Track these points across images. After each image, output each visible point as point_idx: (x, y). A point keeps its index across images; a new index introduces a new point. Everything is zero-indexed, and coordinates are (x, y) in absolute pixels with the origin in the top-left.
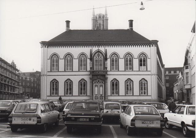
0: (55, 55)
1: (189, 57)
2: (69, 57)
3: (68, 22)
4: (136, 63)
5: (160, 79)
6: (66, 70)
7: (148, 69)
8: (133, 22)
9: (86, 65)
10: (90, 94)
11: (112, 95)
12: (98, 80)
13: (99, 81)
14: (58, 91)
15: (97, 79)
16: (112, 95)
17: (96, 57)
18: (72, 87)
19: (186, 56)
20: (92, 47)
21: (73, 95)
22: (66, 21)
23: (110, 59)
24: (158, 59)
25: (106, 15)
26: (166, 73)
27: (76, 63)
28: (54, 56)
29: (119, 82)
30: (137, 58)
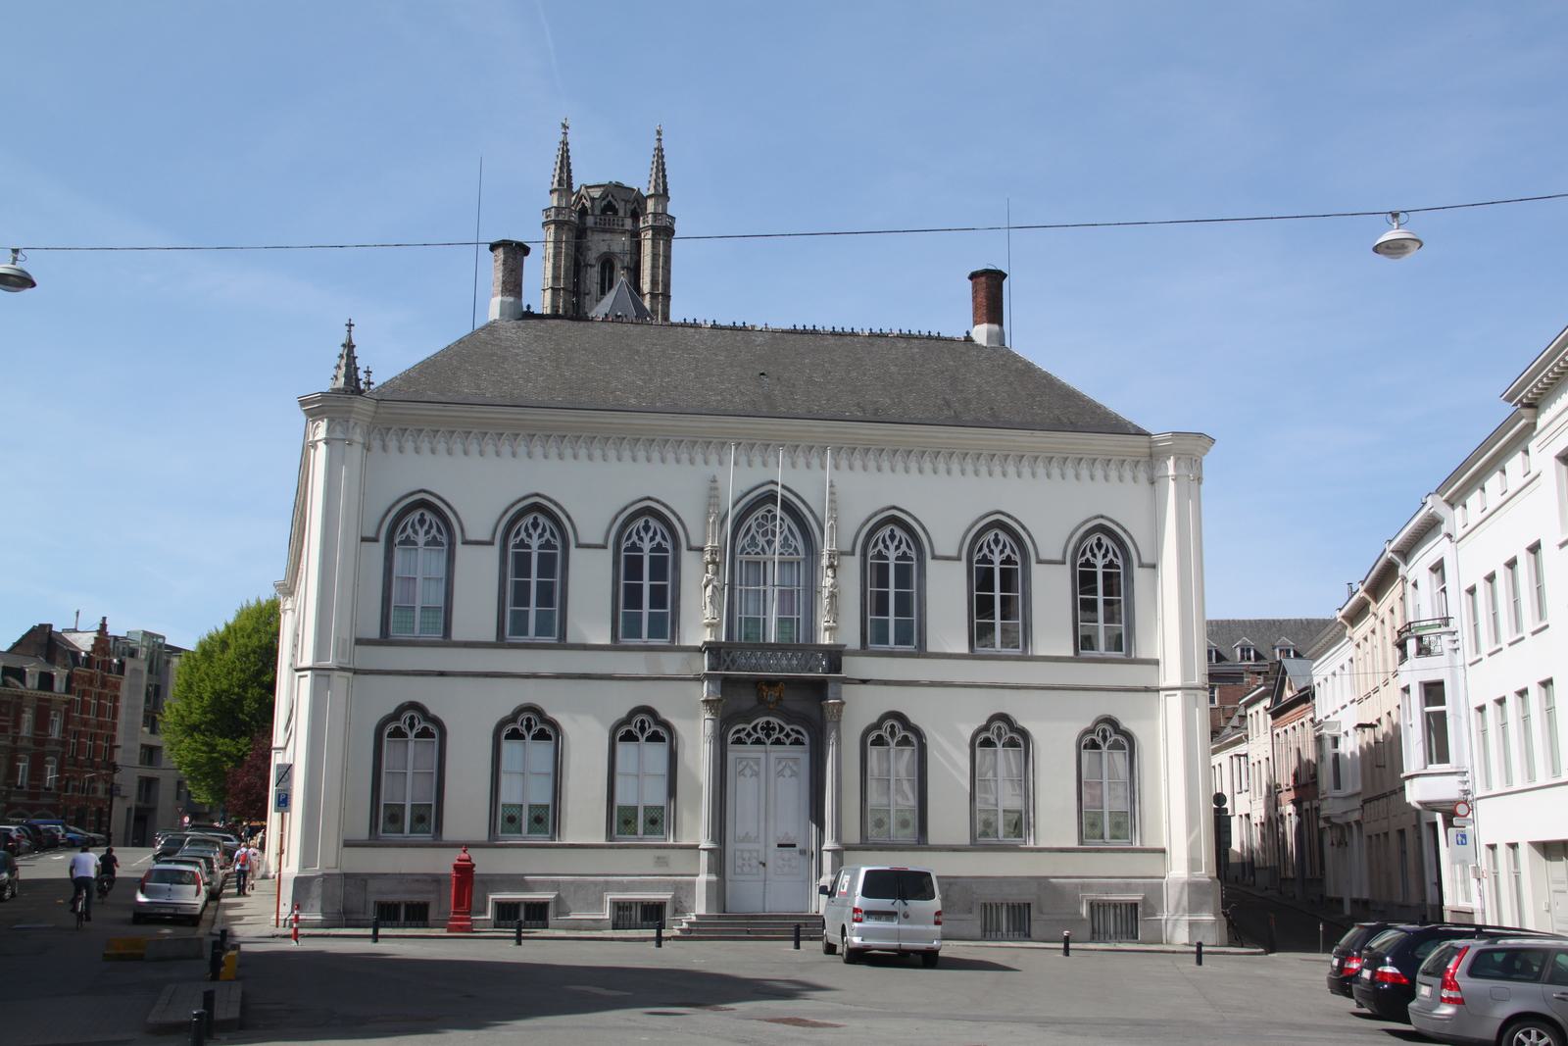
6: (510, 638)
12: (762, 720)
17: (753, 542)
23: (856, 560)
25: (662, 195)
28: (529, 519)
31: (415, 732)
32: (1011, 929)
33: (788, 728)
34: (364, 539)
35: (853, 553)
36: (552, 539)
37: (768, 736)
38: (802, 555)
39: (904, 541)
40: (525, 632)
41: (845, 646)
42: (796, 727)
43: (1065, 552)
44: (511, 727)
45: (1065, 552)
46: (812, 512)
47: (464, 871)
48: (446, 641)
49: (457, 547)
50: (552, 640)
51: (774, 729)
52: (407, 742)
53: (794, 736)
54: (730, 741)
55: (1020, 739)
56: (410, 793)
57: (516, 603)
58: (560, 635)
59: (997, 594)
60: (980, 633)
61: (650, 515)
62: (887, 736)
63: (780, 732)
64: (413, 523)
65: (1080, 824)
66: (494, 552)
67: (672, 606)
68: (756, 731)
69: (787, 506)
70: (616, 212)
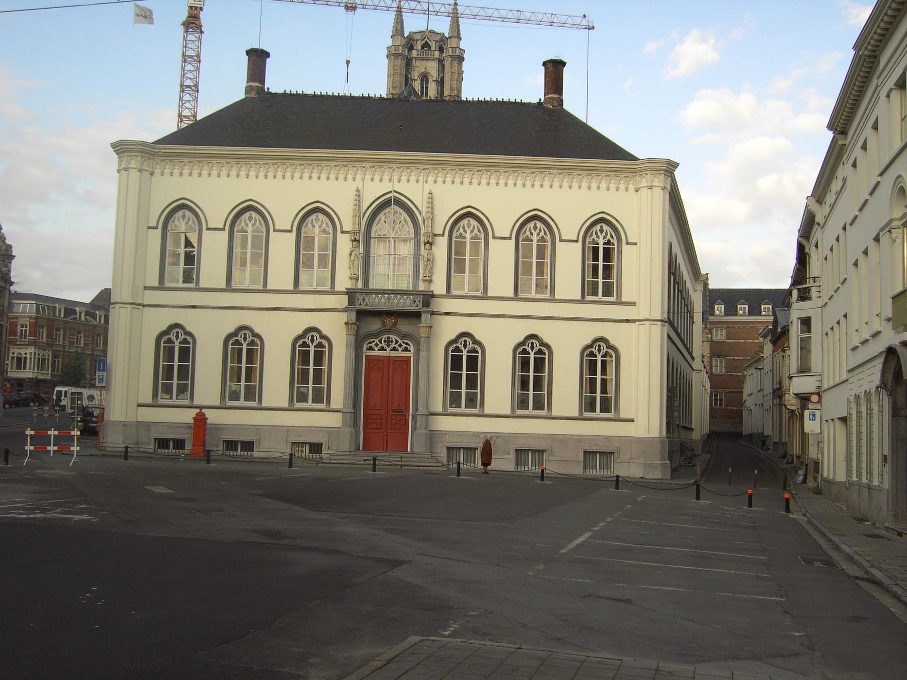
0: (248, 208)
1: (817, 246)
3: (258, 59)
5: (682, 341)
8: (567, 73)
10: (344, 404)
11: (451, 410)
13: (389, 342)
14: (581, 395)
16: (451, 410)
19: (803, 241)
20: (363, 179)
21: (487, 411)
22: (248, 53)
24: (677, 250)
26: (713, 314)
30: (510, 238)
33: (400, 341)
34: (149, 228)
35: (443, 235)
44: (167, 337)
46: (417, 209)
47: (200, 420)
48: (485, 297)
50: (192, 285)
51: (392, 341)
53: (404, 345)
70: (430, 47)
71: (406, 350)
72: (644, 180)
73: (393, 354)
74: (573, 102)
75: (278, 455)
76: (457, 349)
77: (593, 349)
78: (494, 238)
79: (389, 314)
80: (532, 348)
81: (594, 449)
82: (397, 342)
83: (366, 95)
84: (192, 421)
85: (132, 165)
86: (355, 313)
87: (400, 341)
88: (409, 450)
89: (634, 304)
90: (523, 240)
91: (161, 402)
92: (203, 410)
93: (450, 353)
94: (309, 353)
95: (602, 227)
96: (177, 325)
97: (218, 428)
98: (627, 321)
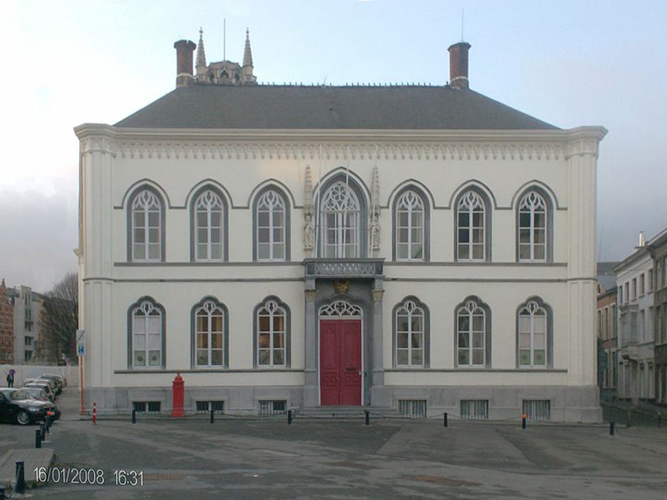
2: (210, 198)
4: (503, 228)
7: (449, 261)
9: (284, 236)
11: (399, 367)
15: (335, 299)
16: (399, 367)
17: (331, 204)
18: (259, 332)
27: (241, 227)
29: (229, 310)
30: (449, 208)
31: (149, 312)
32: (477, 413)
33: (351, 306)
35: (388, 207)
36: (218, 205)
37: (340, 310)
38: (358, 209)
39: (539, 200)
40: (206, 257)
41: (384, 259)
42: (355, 306)
43: (512, 203)
44: (400, 309)
45: (512, 203)
47: (178, 384)
49: (554, 212)
52: (145, 318)
53: (355, 310)
54: (319, 314)
55: (158, 310)
56: (148, 344)
57: (137, 241)
58: (287, 257)
59: (471, 228)
60: (461, 252)
61: (272, 189)
62: (144, 310)
63: (347, 308)
64: (528, 199)
65: (517, 357)
66: (187, 212)
67: (162, 241)
68: (334, 308)
69: (353, 184)
71: (356, 313)
72: (575, 148)
73: (346, 317)
74: (478, 82)
75: (247, 413)
76: (264, 312)
77: (526, 308)
78: (435, 208)
79: (342, 281)
80: (471, 309)
81: (532, 398)
82: (348, 306)
83: (288, 84)
84: (172, 384)
85: (587, 151)
86: (314, 281)
87: (351, 306)
88: (362, 403)
89: (565, 265)
90: (198, 209)
91: (135, 368)
92: (181, 375)
93: (258, 316)
94: (270, 320)
95: (271, 193)
96: (148, 298)
97: (193, 390)
98: (559, 281)
